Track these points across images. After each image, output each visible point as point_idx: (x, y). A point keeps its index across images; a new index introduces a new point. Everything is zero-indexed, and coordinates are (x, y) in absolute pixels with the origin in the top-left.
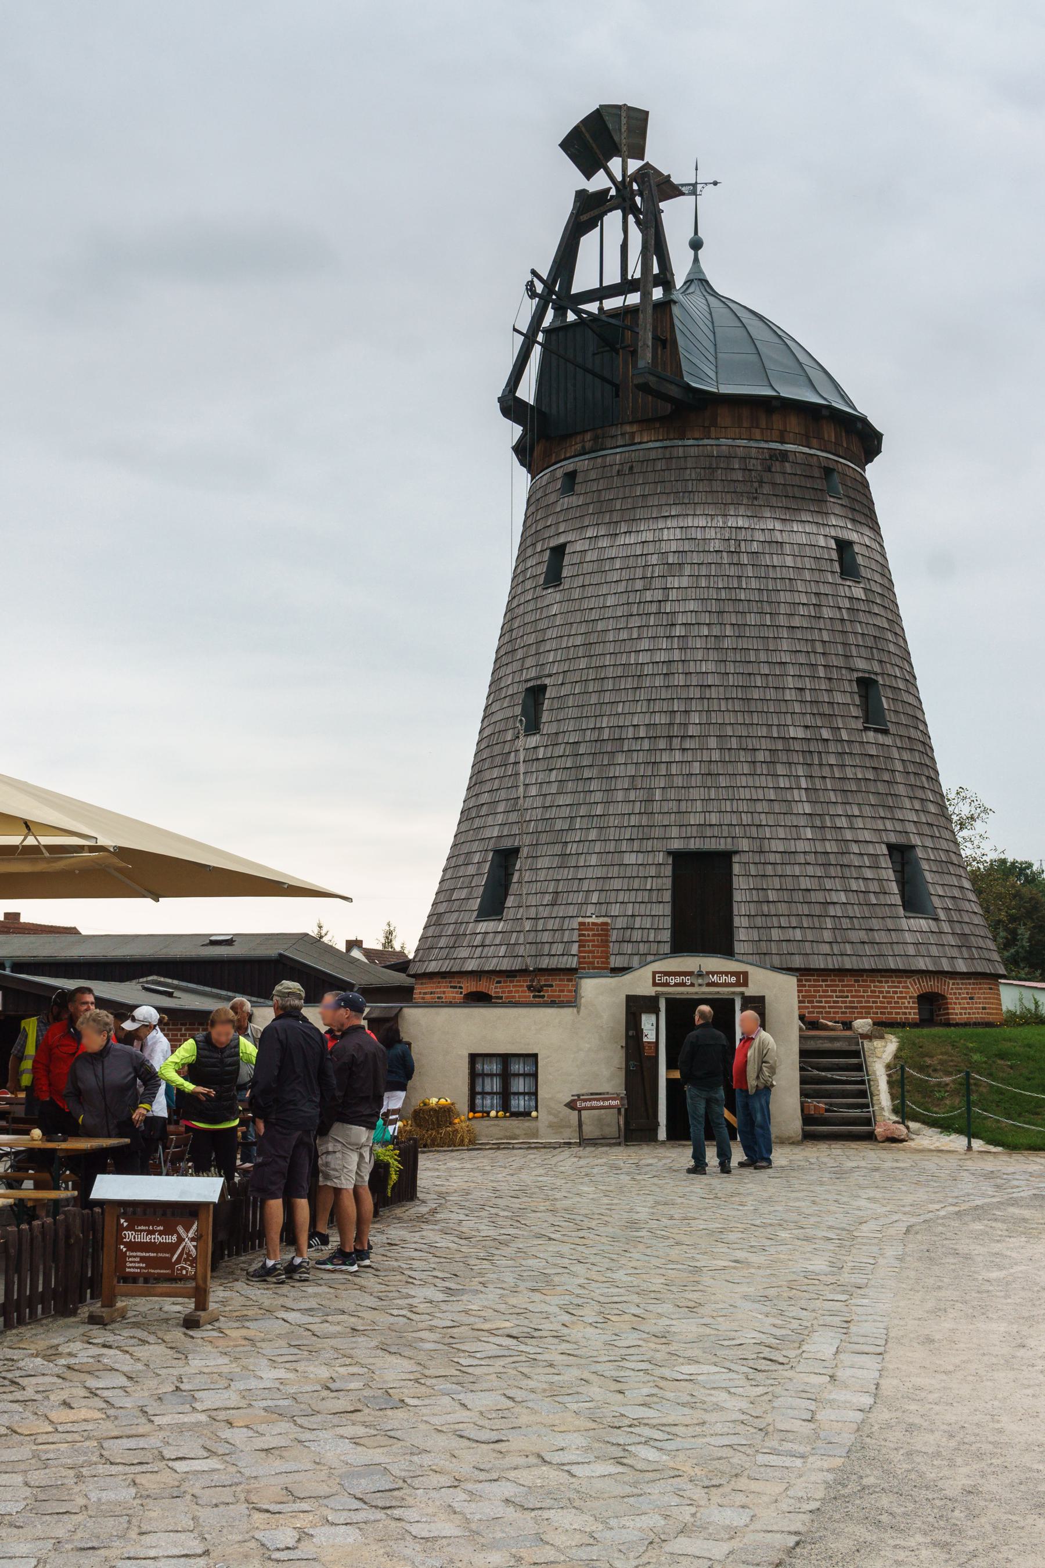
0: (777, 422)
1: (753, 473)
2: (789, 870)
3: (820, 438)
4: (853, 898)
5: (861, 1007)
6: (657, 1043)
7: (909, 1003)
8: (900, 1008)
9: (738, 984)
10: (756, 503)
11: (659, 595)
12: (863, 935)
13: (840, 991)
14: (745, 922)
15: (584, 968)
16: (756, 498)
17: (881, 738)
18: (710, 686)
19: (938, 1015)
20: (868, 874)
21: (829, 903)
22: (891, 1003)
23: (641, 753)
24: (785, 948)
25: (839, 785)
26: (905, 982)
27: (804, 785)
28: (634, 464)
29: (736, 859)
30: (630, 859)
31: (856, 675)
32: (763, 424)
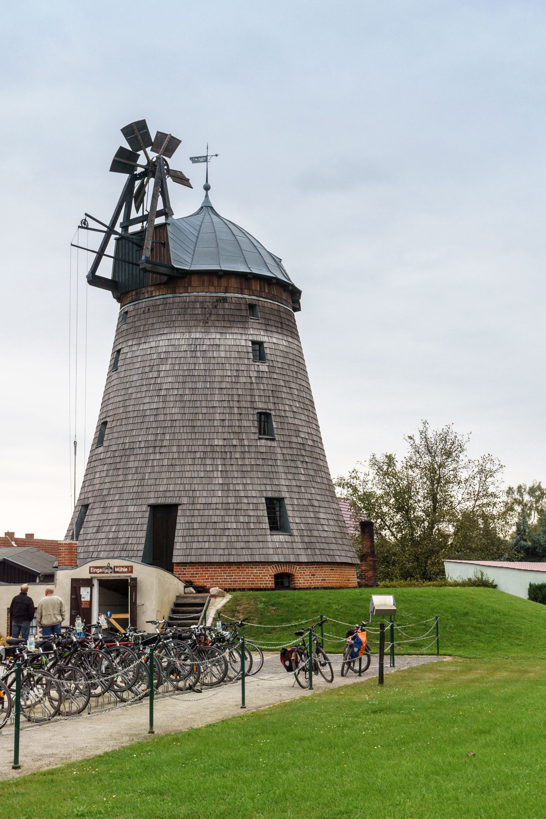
0: (224, 282)
1: (207, 309)
2: (206, 512)
3: (249, 288)
4: (240, 526)
5: (240, 581)
6: (91, 602)
7: (269, 578)
8: (263, 581)
9: (128, 572)
10: (207, 325)
11: (155, 374)
12: (243, 545)
13: (228, 573)
14: (180, 539)
15: (60, 566)
16: (207, 323)
17: (269, 443)
18: (176, 420)
19: (292, 584)
20: (251, 513)
21: (226, 529)
22: (258, 578)
23: (141, 455)
24: (199, 552)
25: (240, 468)
26: (268, 568)
27: (220, 469)
28: (150, 307)
29: (180, 507)
30: (131, 509)
31: (257, 411)
32: (216, 284)
